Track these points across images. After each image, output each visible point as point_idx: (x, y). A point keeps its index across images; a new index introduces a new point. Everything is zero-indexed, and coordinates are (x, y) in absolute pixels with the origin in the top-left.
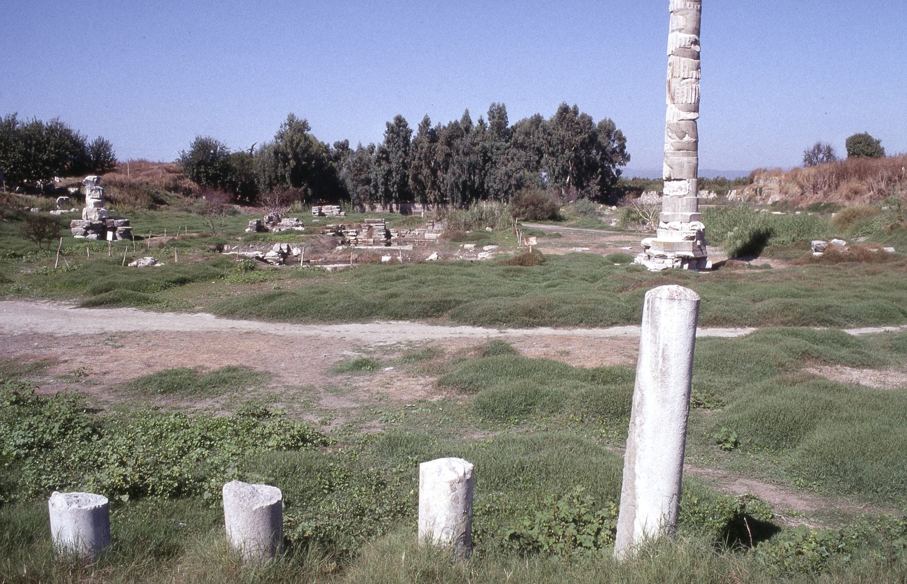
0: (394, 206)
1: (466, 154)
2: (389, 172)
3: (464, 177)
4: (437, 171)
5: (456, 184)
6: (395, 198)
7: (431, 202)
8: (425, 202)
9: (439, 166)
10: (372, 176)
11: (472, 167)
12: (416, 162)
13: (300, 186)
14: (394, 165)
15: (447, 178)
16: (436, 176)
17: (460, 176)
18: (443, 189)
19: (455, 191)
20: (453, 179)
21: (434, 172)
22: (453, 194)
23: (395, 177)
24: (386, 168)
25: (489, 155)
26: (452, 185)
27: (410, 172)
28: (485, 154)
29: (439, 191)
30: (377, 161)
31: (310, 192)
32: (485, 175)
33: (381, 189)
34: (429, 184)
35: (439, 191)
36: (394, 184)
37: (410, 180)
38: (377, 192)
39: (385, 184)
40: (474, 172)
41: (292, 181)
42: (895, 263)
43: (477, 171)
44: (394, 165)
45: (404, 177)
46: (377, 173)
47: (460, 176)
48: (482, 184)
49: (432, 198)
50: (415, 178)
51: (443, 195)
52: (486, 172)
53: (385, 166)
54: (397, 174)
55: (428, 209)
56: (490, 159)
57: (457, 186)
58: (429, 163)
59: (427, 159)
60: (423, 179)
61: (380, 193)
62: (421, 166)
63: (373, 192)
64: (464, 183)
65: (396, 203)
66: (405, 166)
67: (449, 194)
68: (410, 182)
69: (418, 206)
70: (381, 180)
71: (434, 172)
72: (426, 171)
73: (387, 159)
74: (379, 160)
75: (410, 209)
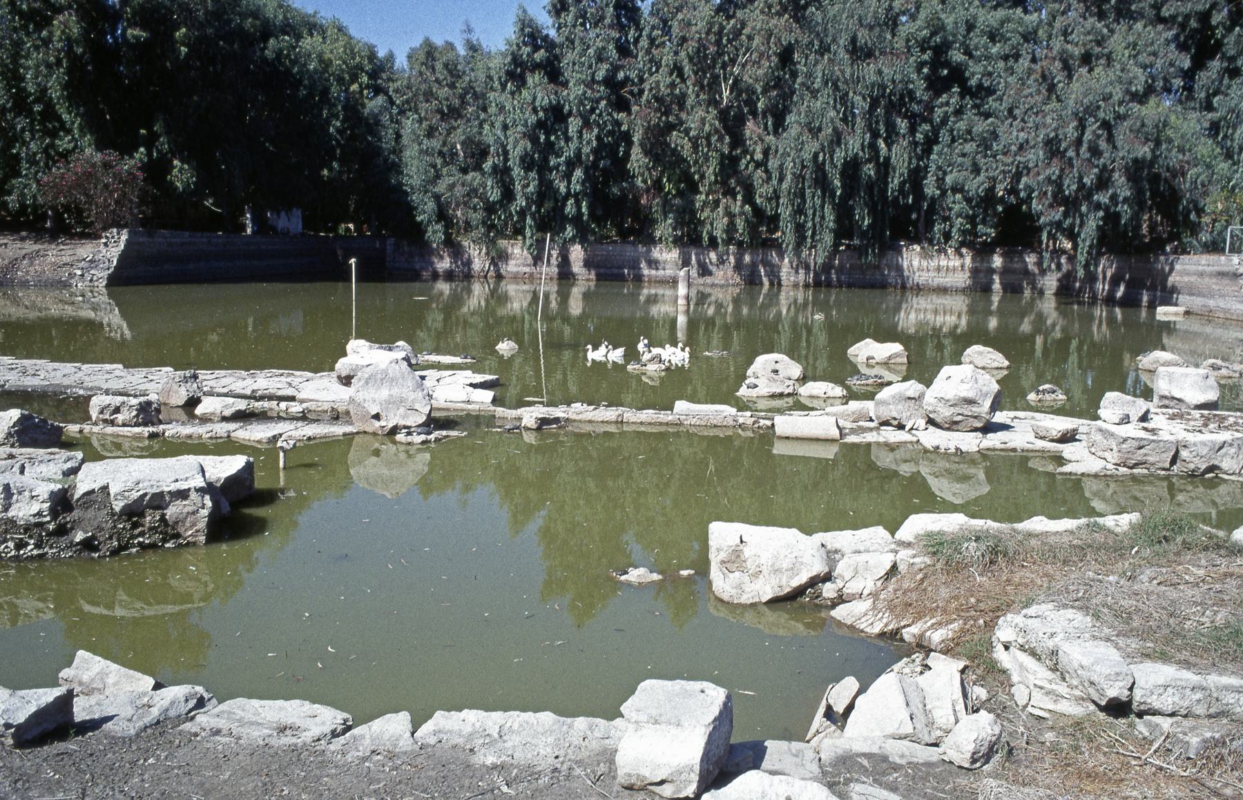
0: (577, 253)
1: (859, 53)
2: (556, 116)
3: (854, 143)
4: (741, 120)
5: (820, 168)
6: (577, 220)
7: (713, 243)
8: (691, 237)
9: (751, 104)
10: (489, 136)
11: (891, 105)
12: (661, 80)
13: (127, 149)
14: (574, 92)
15: (785, 152)
16: (738, 140)
17: (837, 139)
18: (762, 191)
19: (813, 198)
20: (812, 147)
21: (732, 124)
22: (800, 211)
23: (579, 140)
24: (543, 99)
25: (957, 56)
26: (799, 178)
27: (637, 122)
28: (940, 51)
29: (749, 198)
30: (511, 75)
31: (181, 174)
32: (931, 141)
33: (525, 186)
34: (711, 171)
35: (749, 198)
36: (571, 164)
37: (636, 152)
38: (508, 195)
39: (537, 162)
40: (891, 129)
41: (93, 124)
42: (1212, 303)
43: (902, 125)
44: (574, 92)
45: (612, 151)
46: (508, 121)
47: (837, 139)
48: (916, 177)
49: (721, 223)
50: (658, 148)
51: (763, 220)
52: (936, 131)
53: (537, 89)
54: (587, 124)
55: (704, 271)
56: (958, 75)
57: (822, 181)
58: (714, 86)
59: (709, 64)
60: (686, 150)
61: (521, 202)
62: (681, 101)
63: (494, 195)
64: (851, 168)
65: (582, 235)
66: (619, 94)
67: (785, 212)
68: (637, 159)
69: (668, 255)
70: (518, 148)
71: (732, 124)
72: (700, 119)
73: (553, 73)
74: (517, 73)
75: (635, 266)
